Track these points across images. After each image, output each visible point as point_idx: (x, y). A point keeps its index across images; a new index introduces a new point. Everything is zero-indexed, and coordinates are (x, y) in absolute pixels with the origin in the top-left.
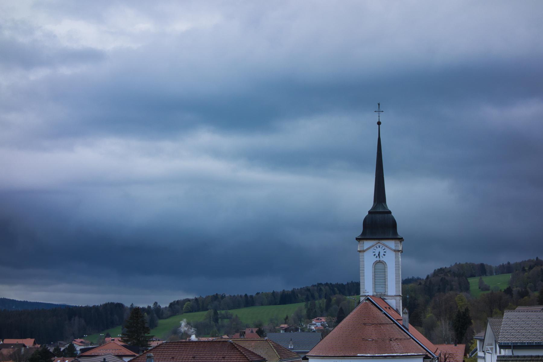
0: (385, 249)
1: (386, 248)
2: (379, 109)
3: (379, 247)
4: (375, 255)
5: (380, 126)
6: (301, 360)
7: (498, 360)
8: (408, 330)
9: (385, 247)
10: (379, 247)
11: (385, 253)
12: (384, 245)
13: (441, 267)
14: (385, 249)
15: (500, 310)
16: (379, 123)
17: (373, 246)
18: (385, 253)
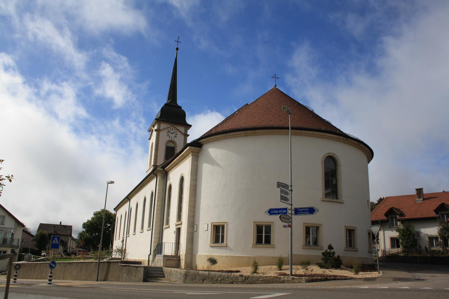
0: (176, 132)
1: (177, 131)
2: (177, 41)
3: (172, 130)
4: (176, 136)
5: (178, 51)
6: (1, 254)
7: (159, 201)
8: (152, 193)
9: (177, 130)
10: (172, 130)
11: (176, 135)
12: (176, 128)
13: (165, 144)
14: (176, 132)
15: (445, 227)
16: (177, 49)
17: (168, 128)
18: (176, 135)
